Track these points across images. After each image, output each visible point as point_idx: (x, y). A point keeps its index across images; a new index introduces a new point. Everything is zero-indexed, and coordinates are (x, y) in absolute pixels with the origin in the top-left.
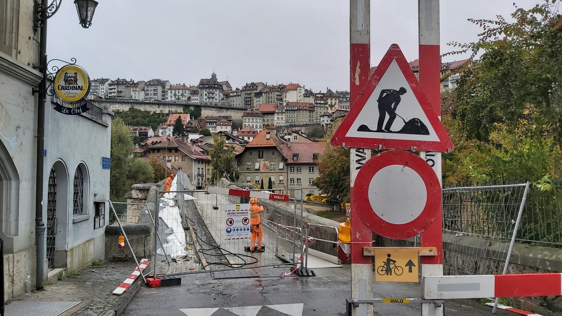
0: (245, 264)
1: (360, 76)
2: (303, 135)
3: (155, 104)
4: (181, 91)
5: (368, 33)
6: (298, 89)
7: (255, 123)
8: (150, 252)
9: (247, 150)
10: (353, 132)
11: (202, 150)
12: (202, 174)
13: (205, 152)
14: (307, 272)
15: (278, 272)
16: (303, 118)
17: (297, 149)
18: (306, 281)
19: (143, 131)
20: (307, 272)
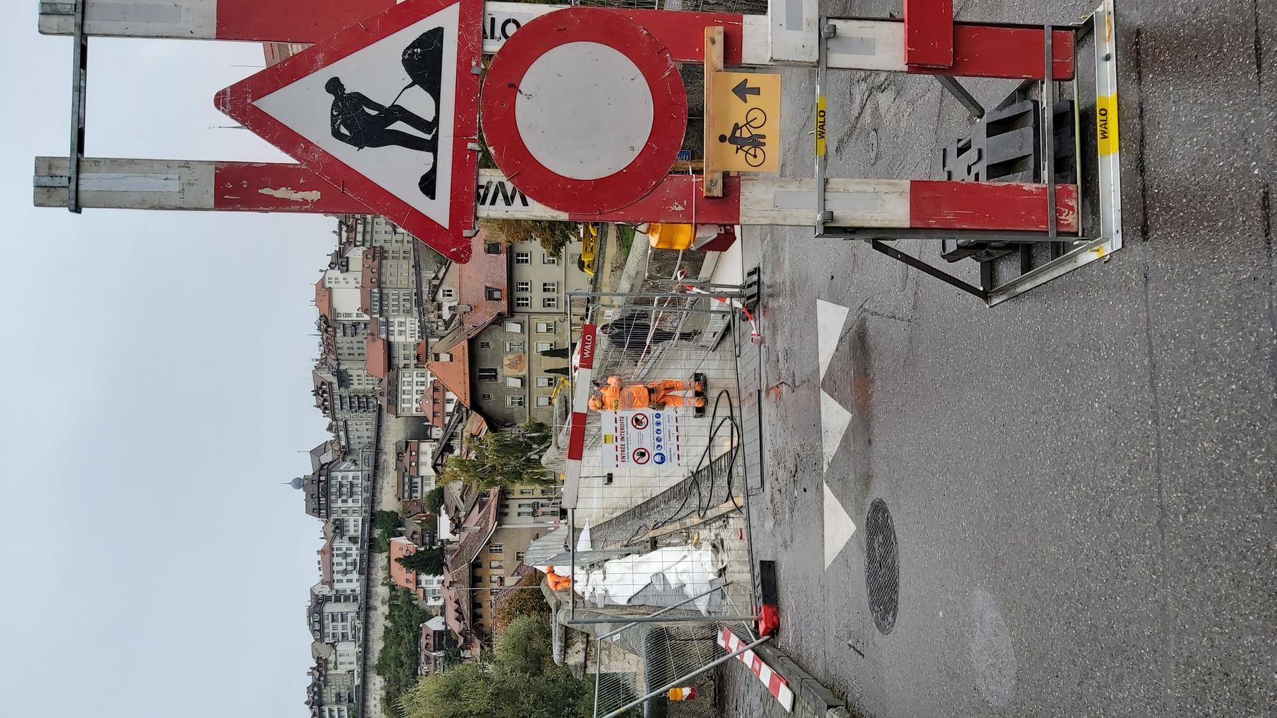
0: (732, 418)
1: (297, 188)
2: (441, 275)
3: (367, 617)
4: (336, 560)
5: (186, 164)
6: (328, 285)
7: (414, 391)
8: (703, 627)
9: (476, 405)
10: (438, 210)
11: (477, 507)
12: (533, 505)
13: (481, 501)
14: (750, 286)
15: (749, 348)
16: (399, 274)
17: (476, 292)
18: (769, 287)
19: (431, 642)
20: (750, 286)
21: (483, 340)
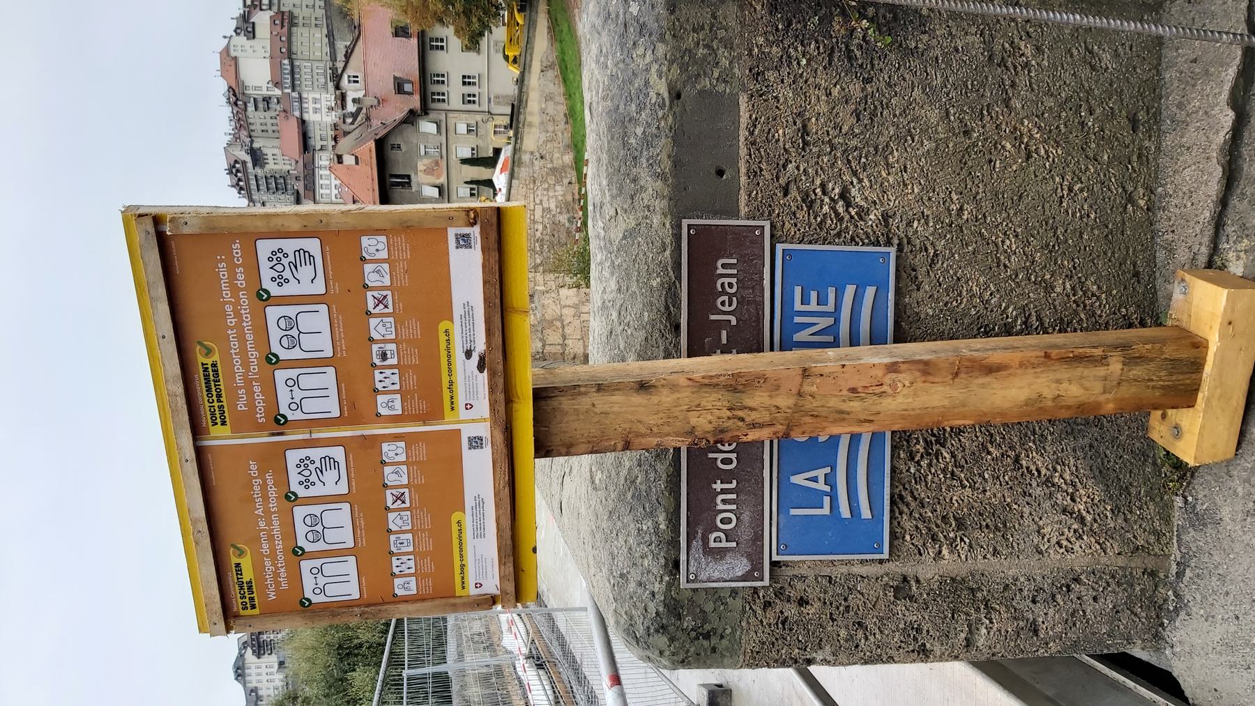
6: (233, 54)
16: (312, 43)
21: (394, 140)
